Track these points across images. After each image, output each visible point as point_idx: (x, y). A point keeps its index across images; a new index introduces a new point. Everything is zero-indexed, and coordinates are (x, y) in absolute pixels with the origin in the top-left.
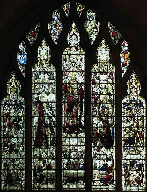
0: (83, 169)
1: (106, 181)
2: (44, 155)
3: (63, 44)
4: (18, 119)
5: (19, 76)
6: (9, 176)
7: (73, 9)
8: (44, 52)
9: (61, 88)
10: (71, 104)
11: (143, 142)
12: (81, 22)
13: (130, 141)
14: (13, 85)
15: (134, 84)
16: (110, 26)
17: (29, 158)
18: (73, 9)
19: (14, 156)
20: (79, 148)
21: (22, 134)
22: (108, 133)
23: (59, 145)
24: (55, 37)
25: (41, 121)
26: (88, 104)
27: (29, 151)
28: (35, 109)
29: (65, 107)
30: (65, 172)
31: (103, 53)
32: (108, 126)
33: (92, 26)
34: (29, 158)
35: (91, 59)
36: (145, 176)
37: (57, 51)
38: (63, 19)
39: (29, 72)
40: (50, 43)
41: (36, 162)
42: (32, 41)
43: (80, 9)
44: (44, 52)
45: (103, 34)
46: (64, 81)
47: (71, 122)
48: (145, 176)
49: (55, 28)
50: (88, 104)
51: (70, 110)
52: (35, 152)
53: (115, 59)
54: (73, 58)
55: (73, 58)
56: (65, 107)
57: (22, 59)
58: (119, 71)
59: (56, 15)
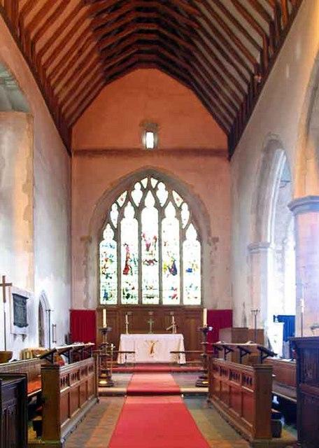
0: (206, 387)
3: (142, 205)
5: (112, 227)
6: (106, 294)
7: (149, 183)
8: (129, 211)
10: (148, 246)
12: (154, 190)
14: (108, 233)
15: (192, 233)
16: (175, 195)
17: (119, 282)
18: (149, 183)
22: (174, 267)
24: (137, 202)
26: (160, 245)
27: (119, 276)
29: (144, 248)
31: (170, 211)
33: (162, 193)
34: (119, 282)
35: (162, 216)
37: (139, 209)
38: (142, 189)
39: (119, 224)
40: (133, 204)
42: (121, 203)
43: (154, 182)
44: (129, 211)
45: (170, 198)
49: (137, 195)
50: (160, 245)
52: (124, 277)
53: (215, 400)
54: (150, 214)
55: (150, 214)
58: (181, 224)
59: (138, 186)
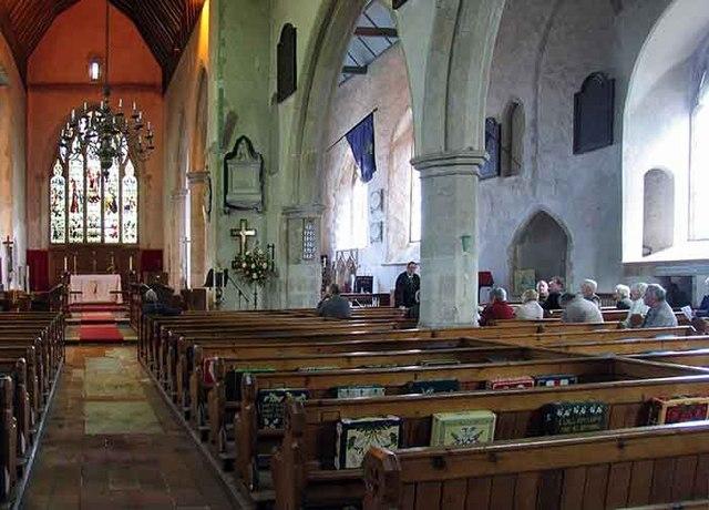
1: (113, 236)
2: (77, 216)
4: (60, 192)
9: (86, 173)
11: (135, 209)
13: (128, 208)
19: (58, 218)
20: (76, 317)
21: (63, 202)
23: (85, 212)
25: (74, 194)
28: (71, 185)
29: (89, 184)
30: (89, 230)
32: (114, 198)
36: (66, 462)
39: (67, 160)
41: (71, 223)
46: (67, 348)
47: (93, 194)
48: (66, 462)
51: (92, 186)
52: (71, 215)
56: (89, 184)
57: (63, 150)
